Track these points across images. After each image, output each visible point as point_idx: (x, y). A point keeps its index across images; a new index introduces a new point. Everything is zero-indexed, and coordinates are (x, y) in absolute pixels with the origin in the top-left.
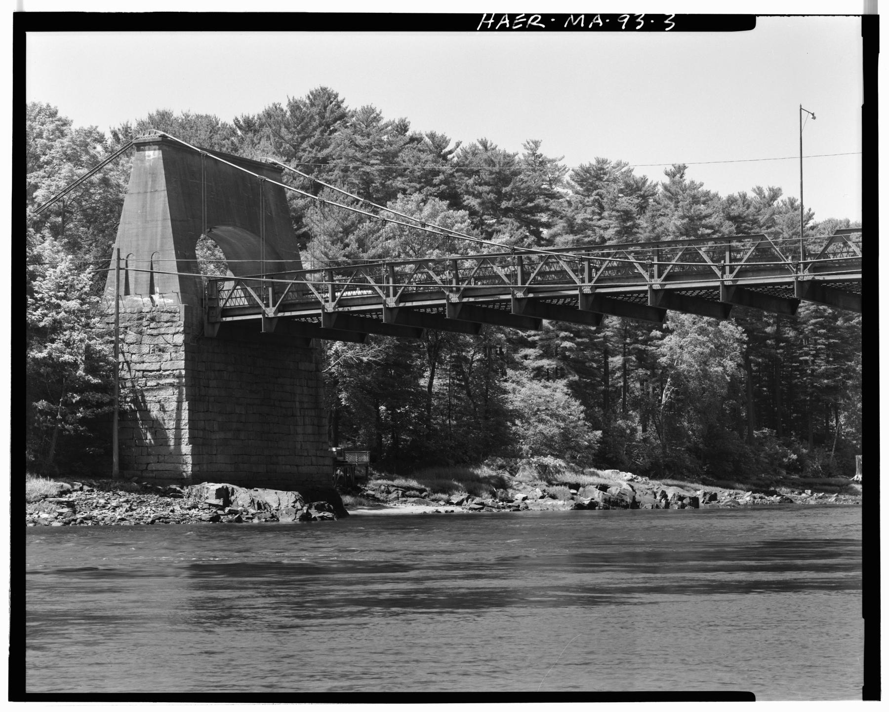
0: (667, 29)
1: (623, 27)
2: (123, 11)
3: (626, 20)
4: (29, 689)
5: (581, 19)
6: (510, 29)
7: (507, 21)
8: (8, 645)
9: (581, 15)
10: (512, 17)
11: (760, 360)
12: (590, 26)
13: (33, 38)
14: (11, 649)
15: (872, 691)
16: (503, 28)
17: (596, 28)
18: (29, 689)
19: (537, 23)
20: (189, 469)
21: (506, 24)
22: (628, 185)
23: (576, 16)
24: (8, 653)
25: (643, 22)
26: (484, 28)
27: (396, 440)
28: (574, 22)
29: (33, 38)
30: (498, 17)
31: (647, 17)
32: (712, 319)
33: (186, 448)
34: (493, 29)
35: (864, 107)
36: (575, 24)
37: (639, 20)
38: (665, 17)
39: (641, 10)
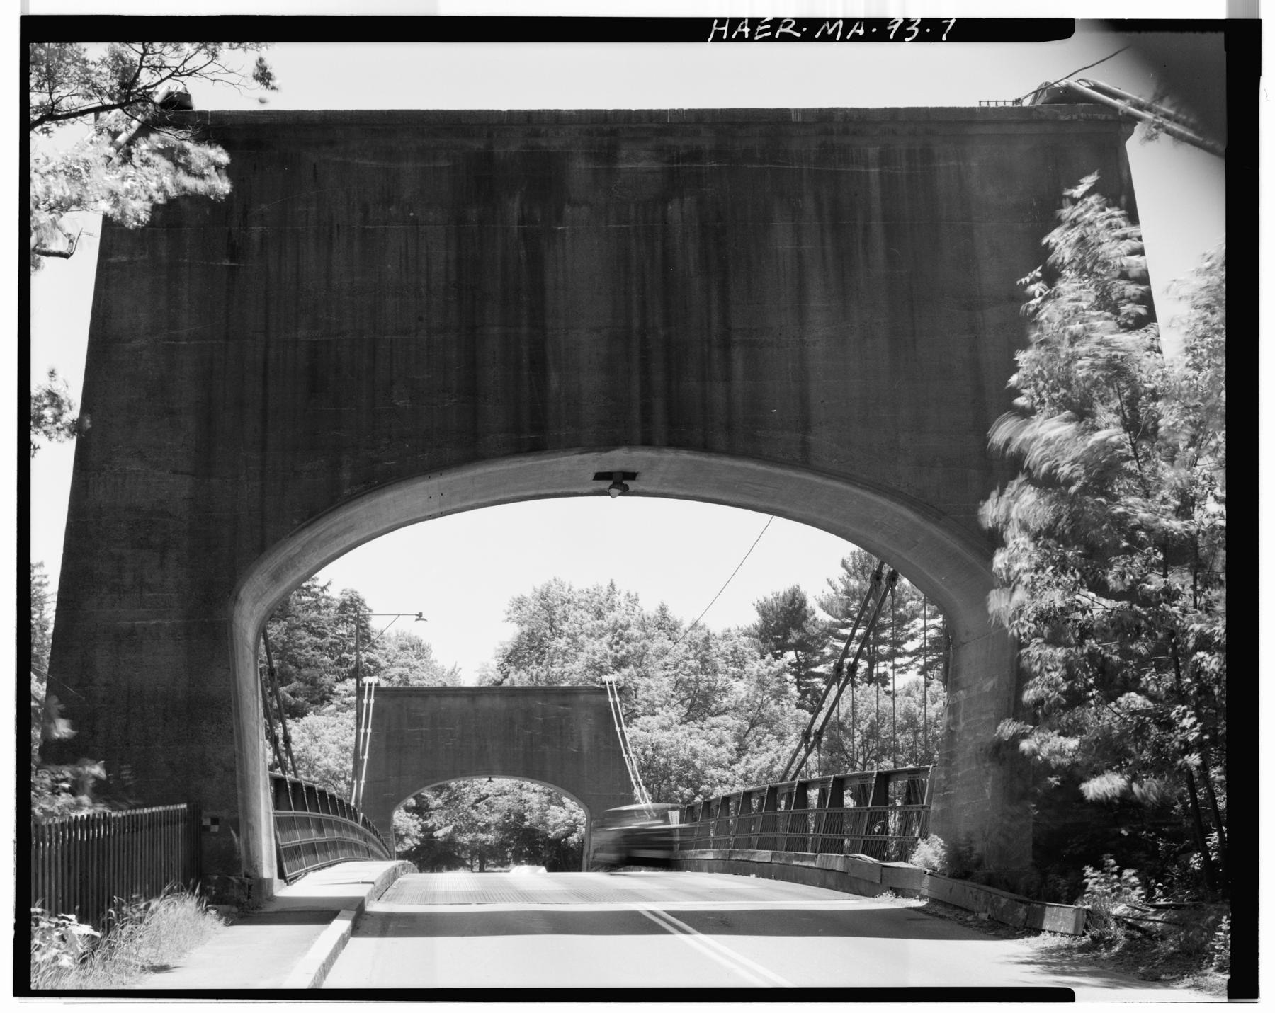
0: (907, 39)
3: (896, 27)
4: (1220, 37)
5: (839, 25)
6: (751, 39)
9: (837, 19)
10: (754, 22)
11: (1167, 829)
12: (734, 36)
13: (36, 982)
16: (741, 38)
19: (791, 29)
22: (328, 770)
23: (833, 21)
25: (917, 31)
26: (718, 38)
27: (649, 774)
30: (735, 22)
31: (925, 22)
33: (366, 757)
34: (729, 40)
35: (1260, 74)
37: (913, 28)
38: (887, 21)
39: (917, 14)
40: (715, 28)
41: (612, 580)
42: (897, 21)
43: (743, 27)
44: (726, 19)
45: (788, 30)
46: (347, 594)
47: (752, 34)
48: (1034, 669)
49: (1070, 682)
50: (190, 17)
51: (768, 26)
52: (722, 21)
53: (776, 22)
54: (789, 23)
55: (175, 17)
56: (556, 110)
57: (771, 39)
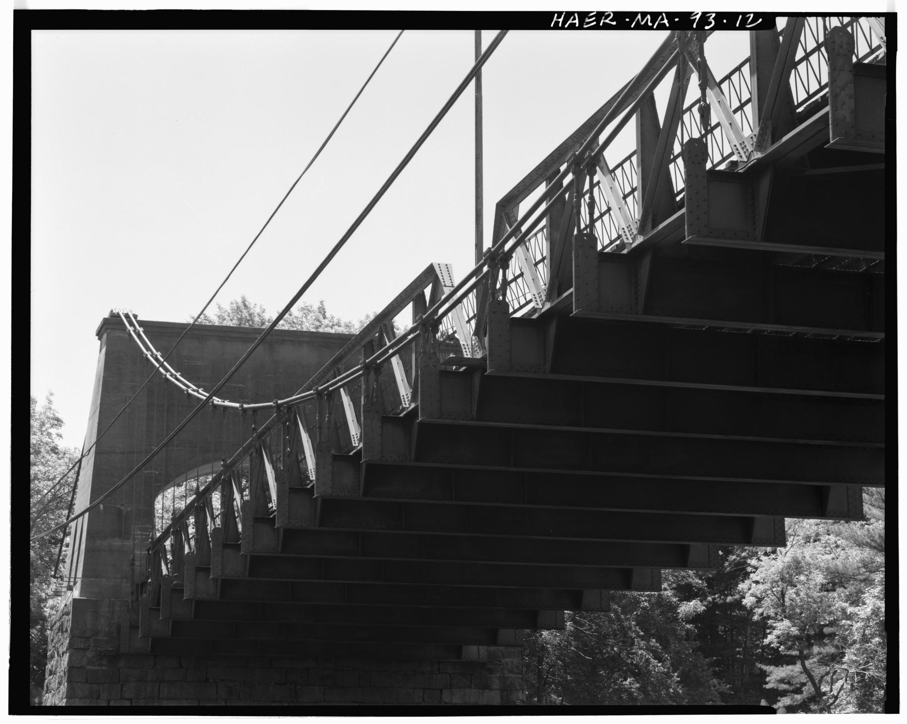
1: (695, 26)
2: (126, 9)
3: (698, 17)
4: (882, 19)
6: (581, 28)
7: (577, 21)
8: (8, 657)
13: (39, 37)
14: (11, 661)
15: (892, 706)
16: (572, 27)
17: (607, 27)
18: (882, 19)
19: (610, 20)
20: (342, 390)
21: (575, 23)
24: (8, 665)
26: (639, 27)
28: (642, 21)
29: (39, 37)
30: (569, 15)
32: (786, 265)
34: (563, 28)
35: (896, 50)
36: (643, 23)
38: (688, 15)
40: (555, 19)
41: (322, 302)
42: (698, 13)
43: (574, 19)
44: (562, 13)
45: (607, 21)
46: (254, 307)
47: (564, 22)
48: (811, 707)
49: (808, 704)
50: (135, 11)
51: (594, 18)
52: (560, 14)
53: (600, 15)
54: (609, 15)
55: (151, 10)
56: (699, 112)
57: (596, 27)
